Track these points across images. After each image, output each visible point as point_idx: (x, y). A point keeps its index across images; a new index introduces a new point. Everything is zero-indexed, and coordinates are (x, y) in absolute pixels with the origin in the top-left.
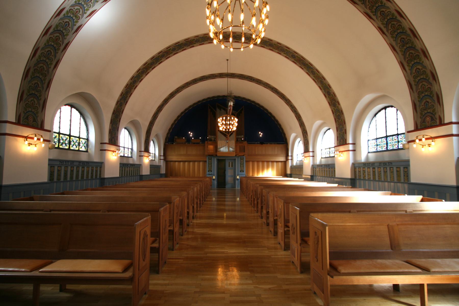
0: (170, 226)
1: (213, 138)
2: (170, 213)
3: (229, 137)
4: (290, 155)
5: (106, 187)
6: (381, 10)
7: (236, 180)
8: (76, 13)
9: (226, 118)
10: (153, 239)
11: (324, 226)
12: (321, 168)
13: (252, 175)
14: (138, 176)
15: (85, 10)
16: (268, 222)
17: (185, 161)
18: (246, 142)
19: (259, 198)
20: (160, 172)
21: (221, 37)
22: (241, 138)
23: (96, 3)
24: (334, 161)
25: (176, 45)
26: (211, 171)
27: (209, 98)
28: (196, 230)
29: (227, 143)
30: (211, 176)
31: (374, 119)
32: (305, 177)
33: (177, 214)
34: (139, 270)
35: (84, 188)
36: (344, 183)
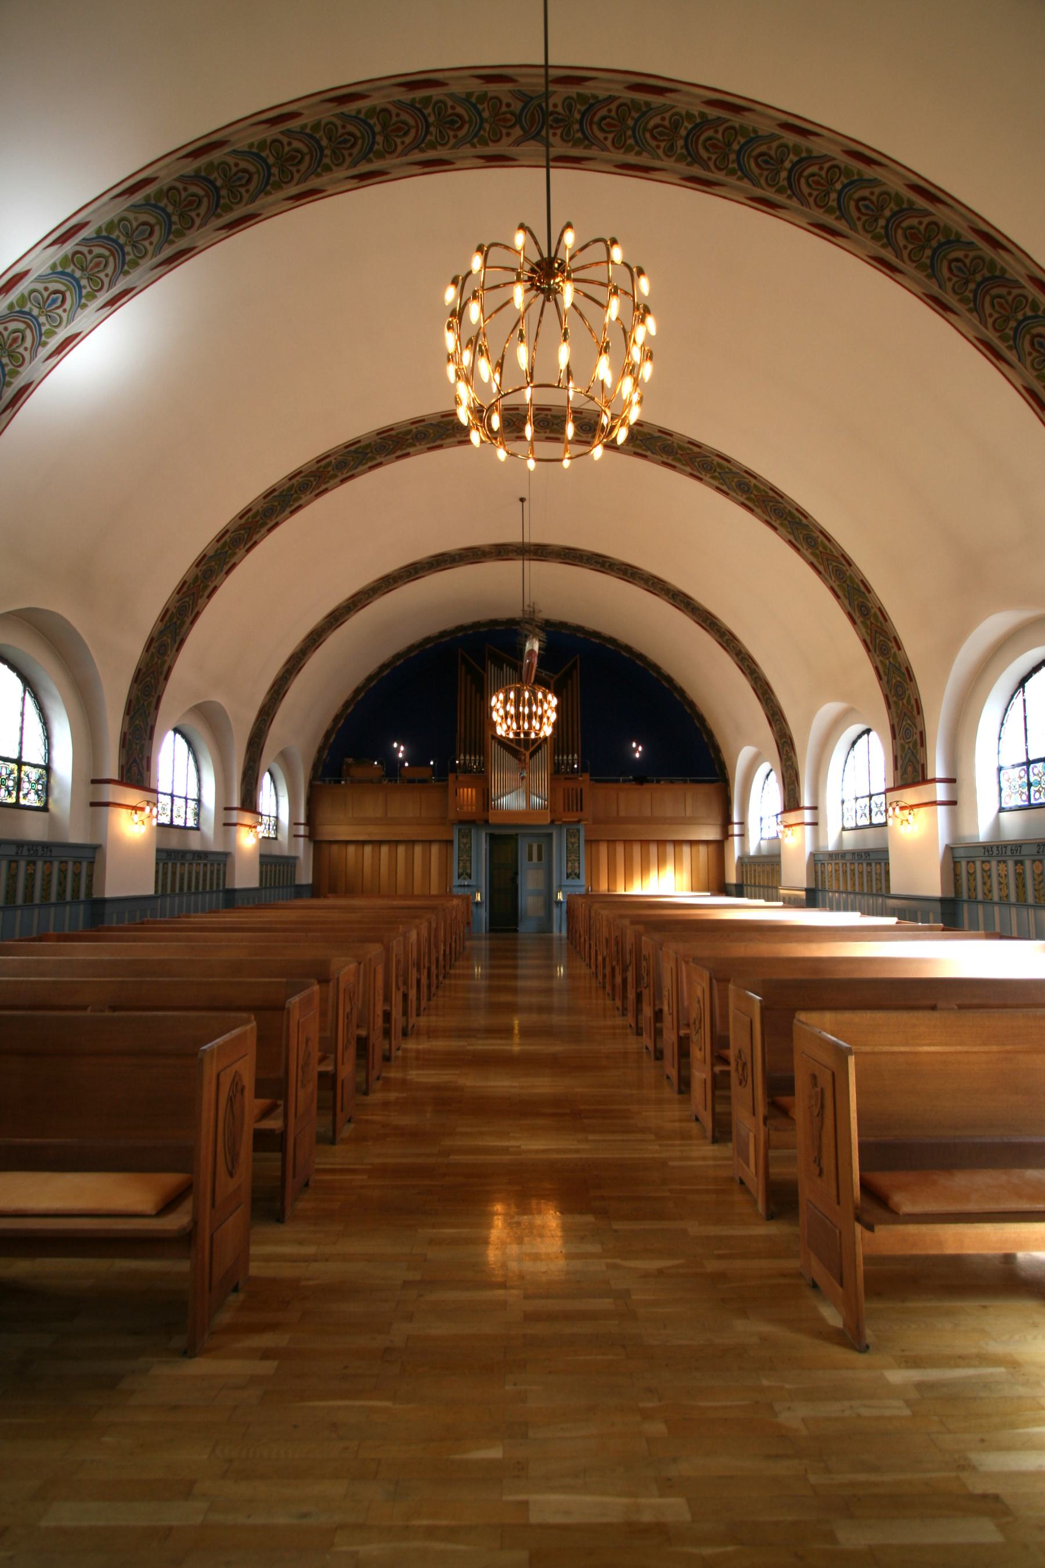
0: (322, 1060)
1: (475, 764)
2: (323, 1014)
3: (527, 759)
4: (736, 818)
5: (110, 929)
6: (1035, 331)
7: (554, 905)
8: (11, 345)
9: (519, 694)
10: (264, 1102)
11: (841, 1055)
12: (840, 862)
13: (609, 890)
14: (218, 891)
15: (41, 335)
16: (658, 1045)
17: (380, 843)
18: (586, 776)
19: (628, 967)
20: (294, 879)
21: (496, 422)
22: (570, 762)
23: (79, 309)
24: (885, 839)
25: (349, 451)
26: (467, 874)
27: (461, 628)
28: (417, 1076)
29: (523, 778)
30: (469, 893)
31: (1018, 701)
32: (787, 894)
33: (348, 1018)
34: (213, 1205)
35: (35, 934)
36: (919, 914)
